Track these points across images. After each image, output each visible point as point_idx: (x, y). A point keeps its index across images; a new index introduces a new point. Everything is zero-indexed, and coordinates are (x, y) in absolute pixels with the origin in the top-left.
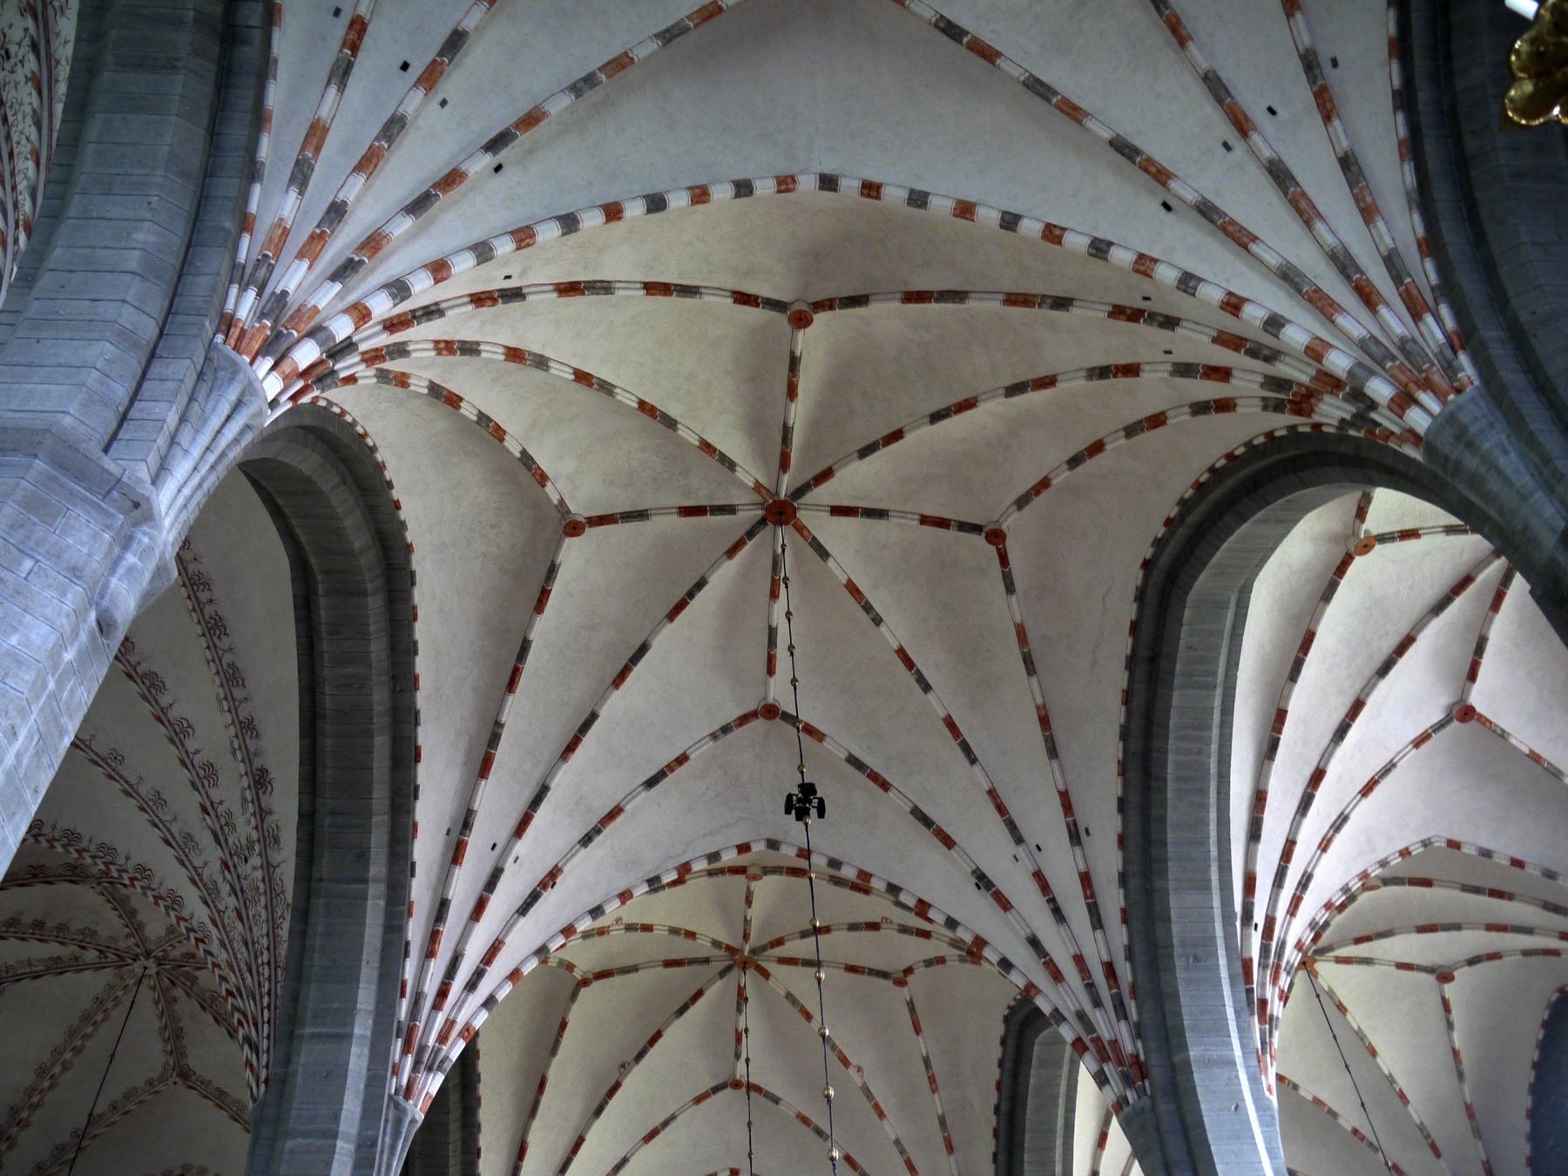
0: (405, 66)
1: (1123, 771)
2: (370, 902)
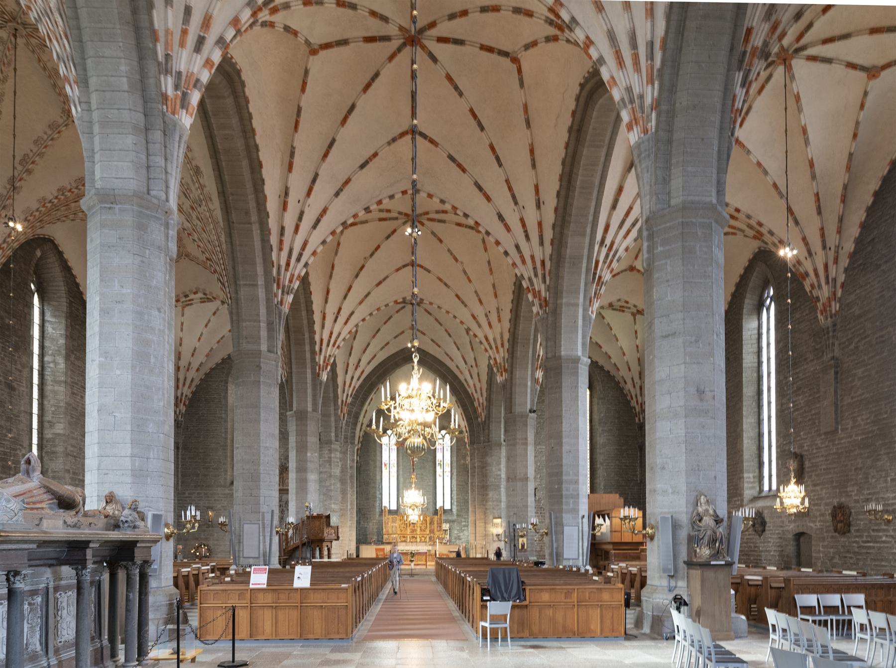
1: (561, 180)
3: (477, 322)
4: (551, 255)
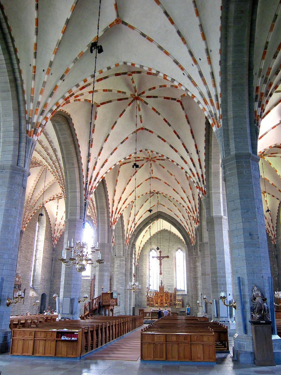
0: (44, 71)
2: (76, 171)
3: (184, 200)
4: (205, 172)
